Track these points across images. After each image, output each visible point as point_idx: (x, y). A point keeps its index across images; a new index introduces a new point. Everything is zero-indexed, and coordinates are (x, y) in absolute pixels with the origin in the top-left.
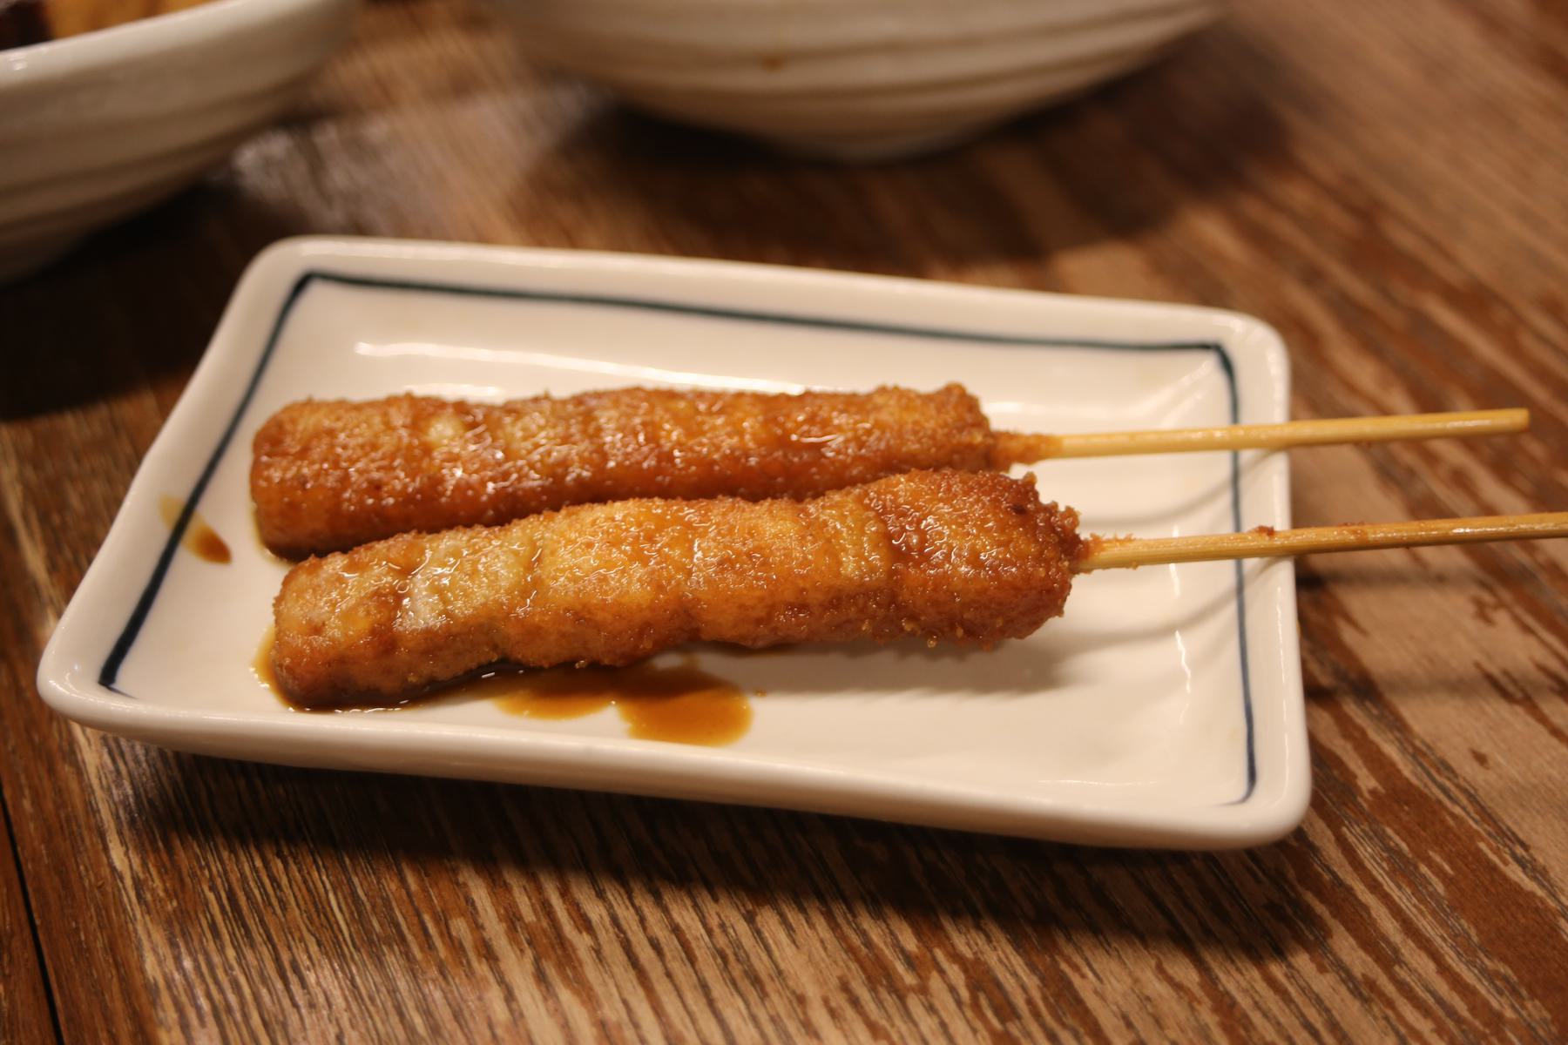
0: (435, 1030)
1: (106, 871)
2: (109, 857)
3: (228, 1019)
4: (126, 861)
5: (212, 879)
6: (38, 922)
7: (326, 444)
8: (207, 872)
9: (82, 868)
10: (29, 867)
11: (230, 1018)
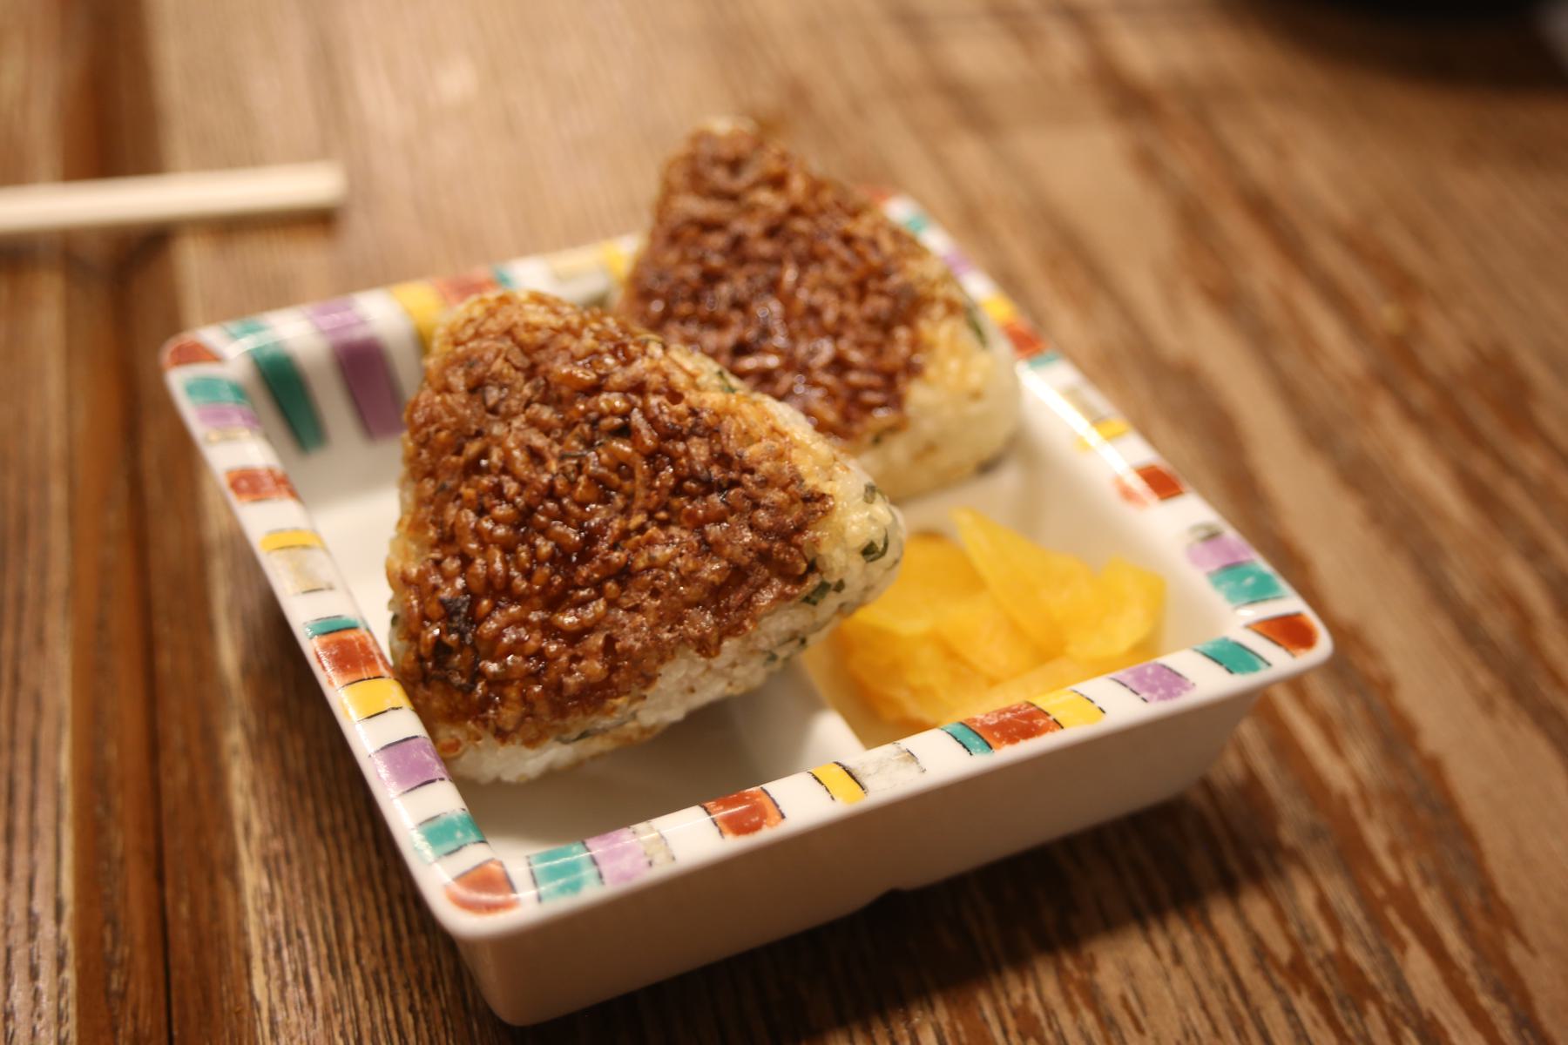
0: (1216, 1032)
1: (245, 998)
2: (250, 984)
3: (1198, 943)
4: (266, 990)
5: (343, 1025)
6: (175, 1033)
7: (415, 599)
8: (340, 1016)
9: (224, 988)
10: (176, 975)
11: (1209, 943)
